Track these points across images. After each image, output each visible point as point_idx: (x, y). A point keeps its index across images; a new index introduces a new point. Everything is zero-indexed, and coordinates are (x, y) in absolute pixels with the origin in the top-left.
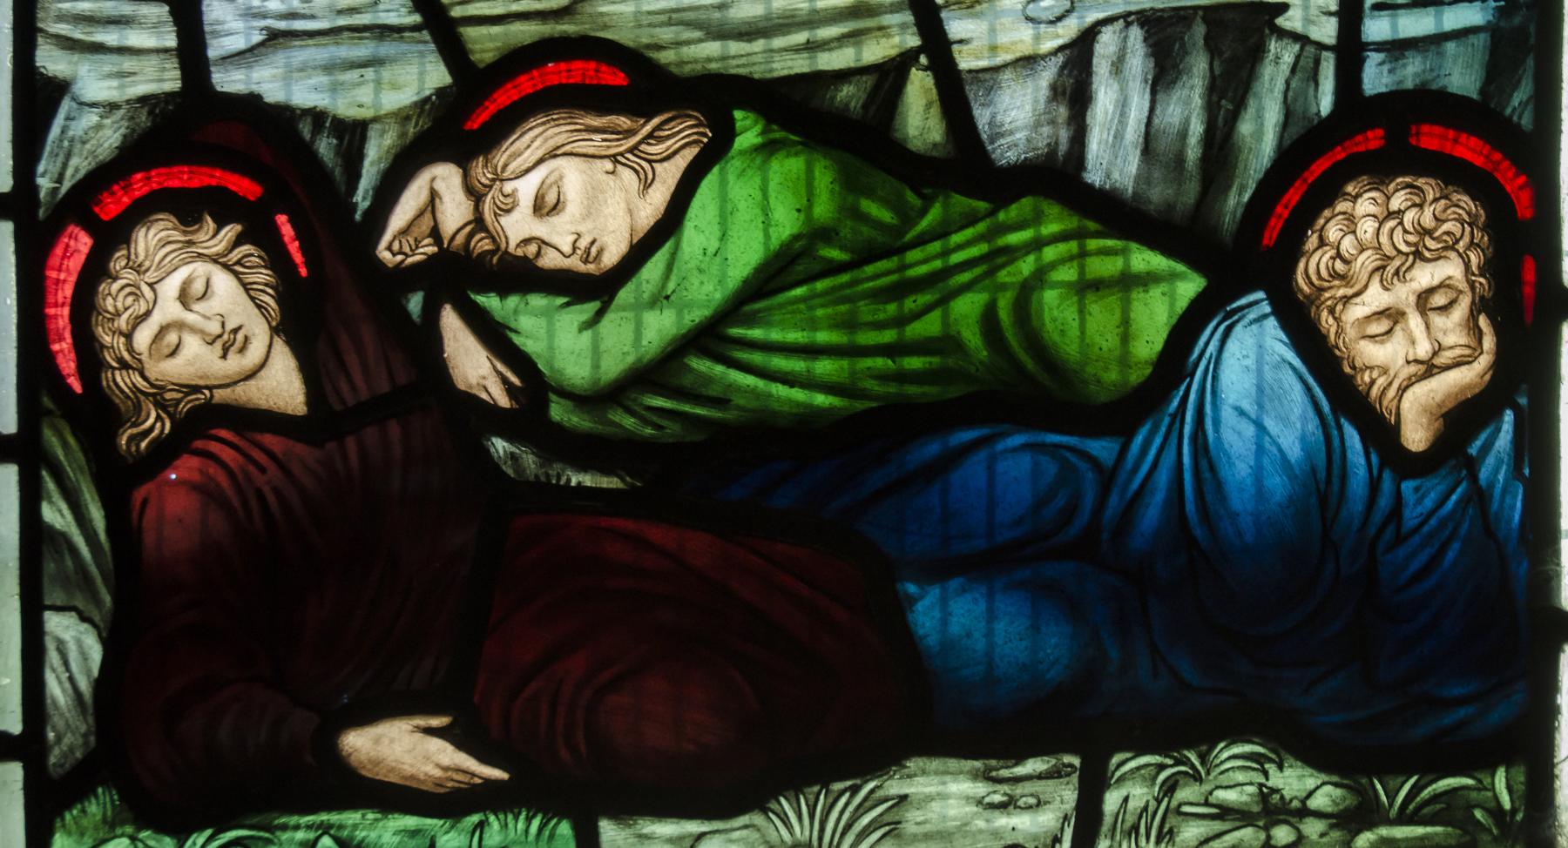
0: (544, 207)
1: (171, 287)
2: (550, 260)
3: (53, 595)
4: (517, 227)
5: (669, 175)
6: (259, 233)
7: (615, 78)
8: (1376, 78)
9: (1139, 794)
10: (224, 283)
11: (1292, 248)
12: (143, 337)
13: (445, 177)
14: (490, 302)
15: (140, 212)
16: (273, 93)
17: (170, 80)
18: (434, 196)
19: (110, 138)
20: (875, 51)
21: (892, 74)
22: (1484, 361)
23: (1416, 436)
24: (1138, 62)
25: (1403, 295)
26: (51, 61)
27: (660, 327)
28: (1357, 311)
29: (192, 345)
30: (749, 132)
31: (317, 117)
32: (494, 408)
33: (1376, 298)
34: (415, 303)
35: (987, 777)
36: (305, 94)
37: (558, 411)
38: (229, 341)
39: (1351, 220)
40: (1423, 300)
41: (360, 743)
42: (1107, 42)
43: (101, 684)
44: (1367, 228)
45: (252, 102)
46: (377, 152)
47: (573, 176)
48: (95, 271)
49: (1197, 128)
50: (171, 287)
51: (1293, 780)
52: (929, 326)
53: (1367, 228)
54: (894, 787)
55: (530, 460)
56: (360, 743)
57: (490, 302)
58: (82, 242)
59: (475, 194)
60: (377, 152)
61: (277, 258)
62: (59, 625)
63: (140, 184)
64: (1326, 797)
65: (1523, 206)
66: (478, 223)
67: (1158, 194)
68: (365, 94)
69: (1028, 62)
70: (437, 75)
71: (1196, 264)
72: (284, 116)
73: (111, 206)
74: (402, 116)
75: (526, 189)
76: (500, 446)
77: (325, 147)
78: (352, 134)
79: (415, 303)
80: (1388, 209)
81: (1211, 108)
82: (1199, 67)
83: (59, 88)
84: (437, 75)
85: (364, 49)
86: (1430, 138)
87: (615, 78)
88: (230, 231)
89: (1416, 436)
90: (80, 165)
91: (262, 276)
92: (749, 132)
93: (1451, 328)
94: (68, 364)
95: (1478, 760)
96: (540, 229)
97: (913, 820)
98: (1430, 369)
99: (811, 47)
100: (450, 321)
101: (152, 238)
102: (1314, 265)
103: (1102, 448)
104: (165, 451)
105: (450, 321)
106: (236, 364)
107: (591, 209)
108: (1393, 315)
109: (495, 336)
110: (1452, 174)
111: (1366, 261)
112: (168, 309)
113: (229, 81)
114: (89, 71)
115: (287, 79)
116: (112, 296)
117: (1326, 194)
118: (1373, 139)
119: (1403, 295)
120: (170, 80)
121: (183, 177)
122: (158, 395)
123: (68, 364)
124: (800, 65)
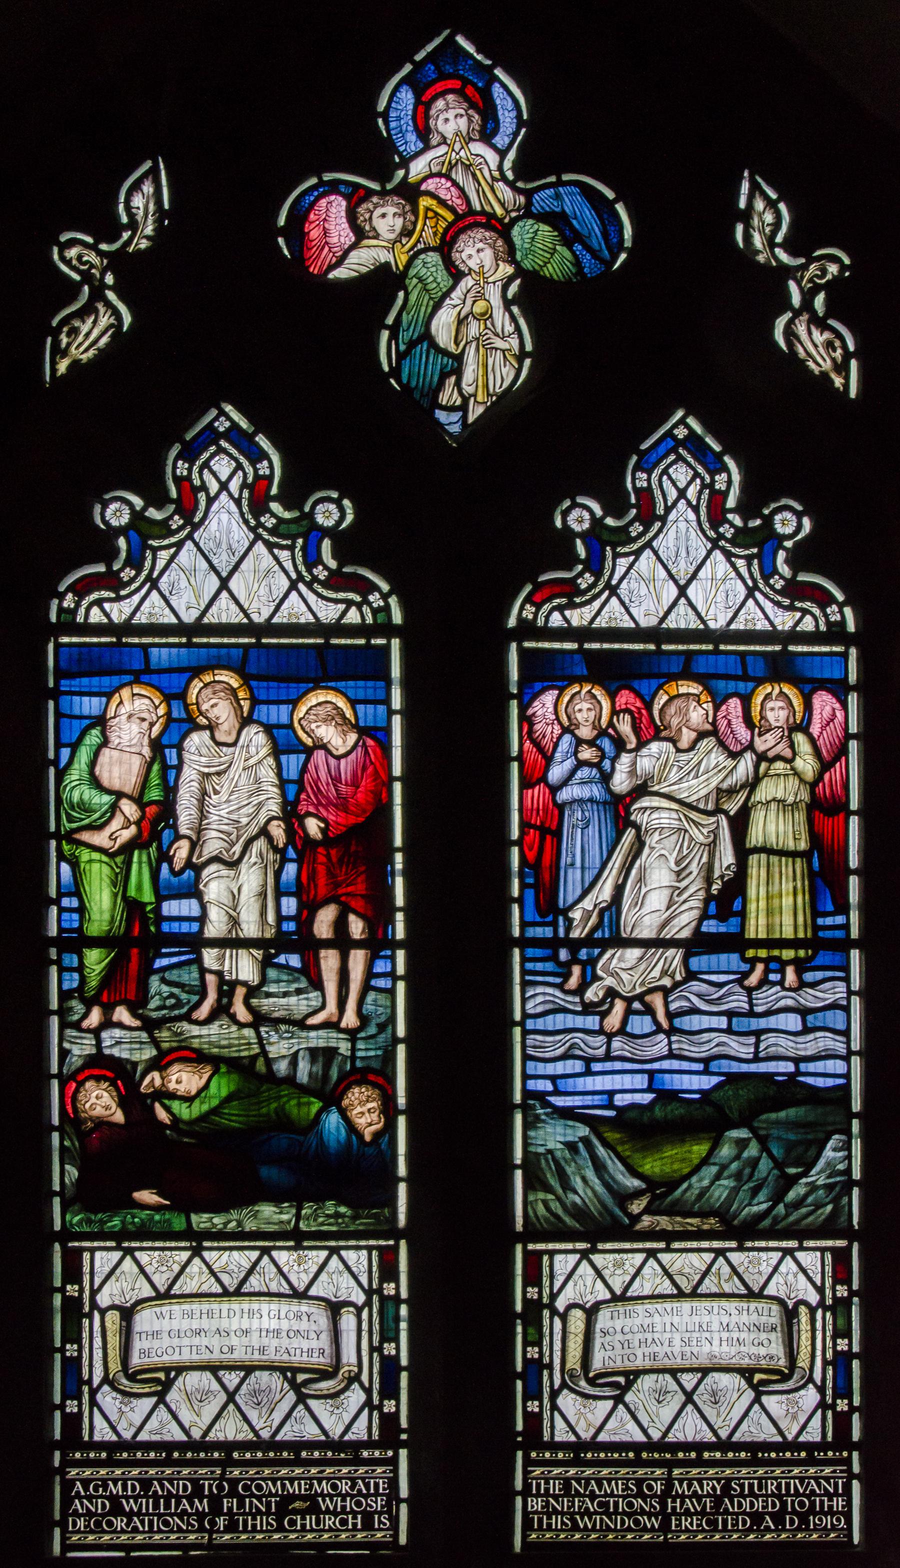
0: (178, 1082)
1: (94, 1094)
2: (179, 1093)
3: (67, 1161)
4: (172, 1086)
5: (206, 1077)
6: (113, 1084)
7: (194, 1056)
8: (359, 1064)
9: (309, 1211)
10: (105, 1094)
11: (341, 1099)
12: (87, 1106)
13: (156, 1075)
14: (166, 1102)
15: (88, 1079)
16: (117, 1054)
17: (94, 1051)
18: (153, 1079)
19: (80, 1062)
20: (252, 1053)
21: (254, 1058)
22: (382, 1124)
23: (368, 1138)
24: (307, 1057)
25: (365, 1109)
26: (66, 1045)
27: (205, 1108)
28: (355, 1112)
29: (98, 1108)
30: (223, 1069)
31: (127, 1060)
32: (166, 1125)
33: (359, 1109)
34: (149, 1101)
35: (276, 1206)
36: (125, 1055)
37: (181, 1126)
38: (107, 1108)
39: (353, 1094)
40: (369, 1110)
41: (137, 1195)
42: (301, 1053)
43: (78, 1180)
44: (357, 1095)
45: (112, 1057)
46: (140, 1069)
47: (184, 1076)
48: (77, 1091)
49: (320, 1073)
50: (94, 1094)
51: (343, 1209)
52: (264, 1110)
53: (357, 1095)
54: (256, 1208)
55: (175, 1136)
56: (137, 1195)
57: (166, 1102)
58: (74, 1085)
59: (163, 1078)
60: (140, 1069)
61: (117, 1089)
62: (67, 1167)
63: (87, 1073)
64: (349, 1213)
65: (390, 1092)
66: (163, 1085)
67: (313, 1085)
68: (138, 1056)
69: (284, 1057)
70: (154, 1052)
71: (320, 1099)
72: (119, 1060)
73: (80, 1078)
74: (146, 1061)
75: (174, 1078)
76: (168, 1132)
77: (129, 1067)
78: (135, 1064)
79: (149, 1101)
80: (805, 783)
81: (323, 1070)
82: (321, 1059)
83: (68, 1052)
84: (154, 1052)
85: (137, 1046)
86: (371, 1077)
87: (194, 1056)
88: (107, 1084)
89: (368, 1138)
90: (73, 1068)
91: (115, 1094)
92: (223, 1069)
93: (375, 1117)
94: (70, 1110)
95: (382, 1206)
96: (177, 1087)
97: (260, 1216)
98: (370, 1125)
99: (240, 1051)
100: (157, 1105)
101: (88, 1085)
102: (345, 1102)
103: (301, 1138)
104: (92, 1130)
105: (157, 1105)
106: (108, 1112)
107: (189, 1081)
108: (363, 1113)
109: (168, 1109)
110: (375, 1085)
111: (356, 1102)
112: (93, 1100)
113: (107, 1052)
114: (216, 792)
115: (121, 1051)
116: (81, 1096)
117: (348, 1087)
118: (358, 1077)
119: (365, 1109)
120: (94, 1051)
121: (96, 1072)
122: (91, 1119)
123: (70, 1110)
124: (236, 1055)
